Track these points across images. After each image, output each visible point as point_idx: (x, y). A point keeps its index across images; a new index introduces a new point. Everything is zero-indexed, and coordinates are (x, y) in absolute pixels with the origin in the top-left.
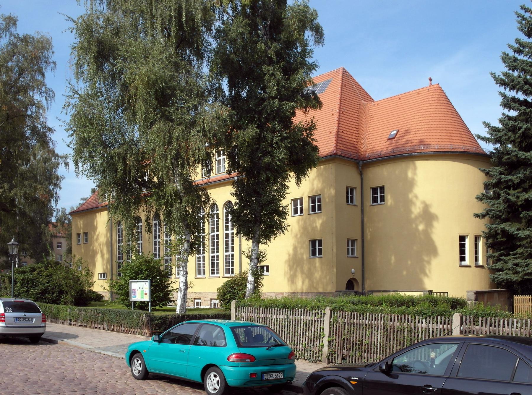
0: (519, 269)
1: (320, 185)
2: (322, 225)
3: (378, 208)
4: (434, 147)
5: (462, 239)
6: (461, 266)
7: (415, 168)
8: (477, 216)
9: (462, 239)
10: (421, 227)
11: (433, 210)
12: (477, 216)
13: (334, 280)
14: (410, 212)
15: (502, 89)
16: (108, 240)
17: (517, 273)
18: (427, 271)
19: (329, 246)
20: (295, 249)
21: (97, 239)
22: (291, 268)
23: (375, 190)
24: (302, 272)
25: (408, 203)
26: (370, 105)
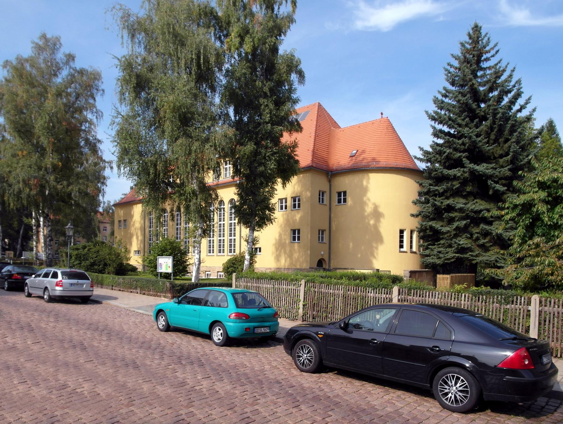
0: (441, 255)
1: (299, 189)
2: (300, 218)
3: (342, 207)
4: (383, 164)
5: (402, 232)
6: (400, 252)
7: (369, 179)
8: (413, 215)
9: (402, 232)
10: (372, 222)
11: (381, 210)
12: (413, 215)
13: (309, 259)
14: (363, 210)
15: (433, 123)
16: (141, 225)
17: (440, 258)
18: (375, 254)
19: (306, 235)
20: (280, 235)
21: (133, 225)
22: (277, 249)
23: (339, 194)
24: (285, 253)
25: (363, 204)
26: (338, 130)
